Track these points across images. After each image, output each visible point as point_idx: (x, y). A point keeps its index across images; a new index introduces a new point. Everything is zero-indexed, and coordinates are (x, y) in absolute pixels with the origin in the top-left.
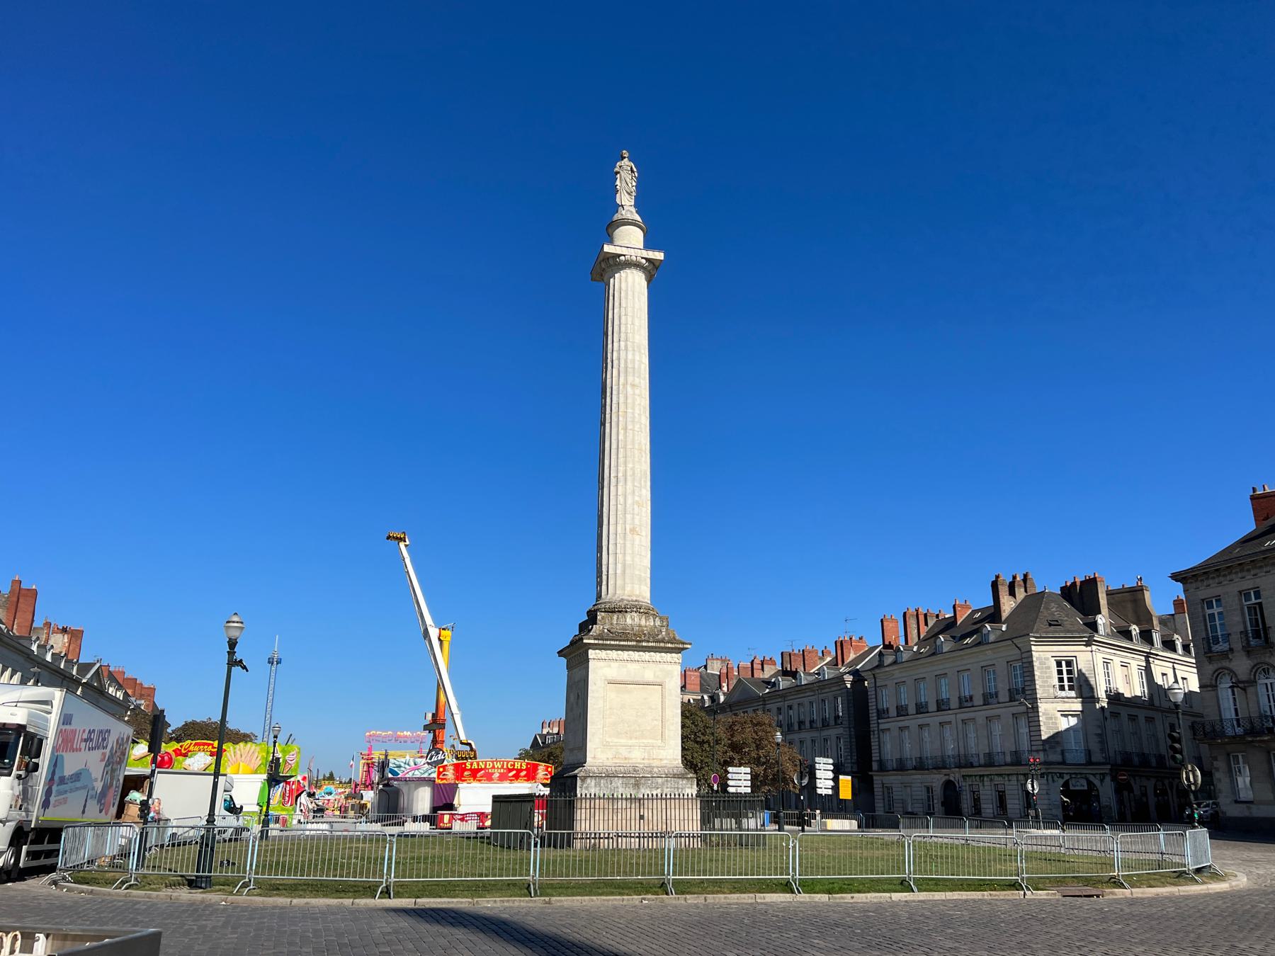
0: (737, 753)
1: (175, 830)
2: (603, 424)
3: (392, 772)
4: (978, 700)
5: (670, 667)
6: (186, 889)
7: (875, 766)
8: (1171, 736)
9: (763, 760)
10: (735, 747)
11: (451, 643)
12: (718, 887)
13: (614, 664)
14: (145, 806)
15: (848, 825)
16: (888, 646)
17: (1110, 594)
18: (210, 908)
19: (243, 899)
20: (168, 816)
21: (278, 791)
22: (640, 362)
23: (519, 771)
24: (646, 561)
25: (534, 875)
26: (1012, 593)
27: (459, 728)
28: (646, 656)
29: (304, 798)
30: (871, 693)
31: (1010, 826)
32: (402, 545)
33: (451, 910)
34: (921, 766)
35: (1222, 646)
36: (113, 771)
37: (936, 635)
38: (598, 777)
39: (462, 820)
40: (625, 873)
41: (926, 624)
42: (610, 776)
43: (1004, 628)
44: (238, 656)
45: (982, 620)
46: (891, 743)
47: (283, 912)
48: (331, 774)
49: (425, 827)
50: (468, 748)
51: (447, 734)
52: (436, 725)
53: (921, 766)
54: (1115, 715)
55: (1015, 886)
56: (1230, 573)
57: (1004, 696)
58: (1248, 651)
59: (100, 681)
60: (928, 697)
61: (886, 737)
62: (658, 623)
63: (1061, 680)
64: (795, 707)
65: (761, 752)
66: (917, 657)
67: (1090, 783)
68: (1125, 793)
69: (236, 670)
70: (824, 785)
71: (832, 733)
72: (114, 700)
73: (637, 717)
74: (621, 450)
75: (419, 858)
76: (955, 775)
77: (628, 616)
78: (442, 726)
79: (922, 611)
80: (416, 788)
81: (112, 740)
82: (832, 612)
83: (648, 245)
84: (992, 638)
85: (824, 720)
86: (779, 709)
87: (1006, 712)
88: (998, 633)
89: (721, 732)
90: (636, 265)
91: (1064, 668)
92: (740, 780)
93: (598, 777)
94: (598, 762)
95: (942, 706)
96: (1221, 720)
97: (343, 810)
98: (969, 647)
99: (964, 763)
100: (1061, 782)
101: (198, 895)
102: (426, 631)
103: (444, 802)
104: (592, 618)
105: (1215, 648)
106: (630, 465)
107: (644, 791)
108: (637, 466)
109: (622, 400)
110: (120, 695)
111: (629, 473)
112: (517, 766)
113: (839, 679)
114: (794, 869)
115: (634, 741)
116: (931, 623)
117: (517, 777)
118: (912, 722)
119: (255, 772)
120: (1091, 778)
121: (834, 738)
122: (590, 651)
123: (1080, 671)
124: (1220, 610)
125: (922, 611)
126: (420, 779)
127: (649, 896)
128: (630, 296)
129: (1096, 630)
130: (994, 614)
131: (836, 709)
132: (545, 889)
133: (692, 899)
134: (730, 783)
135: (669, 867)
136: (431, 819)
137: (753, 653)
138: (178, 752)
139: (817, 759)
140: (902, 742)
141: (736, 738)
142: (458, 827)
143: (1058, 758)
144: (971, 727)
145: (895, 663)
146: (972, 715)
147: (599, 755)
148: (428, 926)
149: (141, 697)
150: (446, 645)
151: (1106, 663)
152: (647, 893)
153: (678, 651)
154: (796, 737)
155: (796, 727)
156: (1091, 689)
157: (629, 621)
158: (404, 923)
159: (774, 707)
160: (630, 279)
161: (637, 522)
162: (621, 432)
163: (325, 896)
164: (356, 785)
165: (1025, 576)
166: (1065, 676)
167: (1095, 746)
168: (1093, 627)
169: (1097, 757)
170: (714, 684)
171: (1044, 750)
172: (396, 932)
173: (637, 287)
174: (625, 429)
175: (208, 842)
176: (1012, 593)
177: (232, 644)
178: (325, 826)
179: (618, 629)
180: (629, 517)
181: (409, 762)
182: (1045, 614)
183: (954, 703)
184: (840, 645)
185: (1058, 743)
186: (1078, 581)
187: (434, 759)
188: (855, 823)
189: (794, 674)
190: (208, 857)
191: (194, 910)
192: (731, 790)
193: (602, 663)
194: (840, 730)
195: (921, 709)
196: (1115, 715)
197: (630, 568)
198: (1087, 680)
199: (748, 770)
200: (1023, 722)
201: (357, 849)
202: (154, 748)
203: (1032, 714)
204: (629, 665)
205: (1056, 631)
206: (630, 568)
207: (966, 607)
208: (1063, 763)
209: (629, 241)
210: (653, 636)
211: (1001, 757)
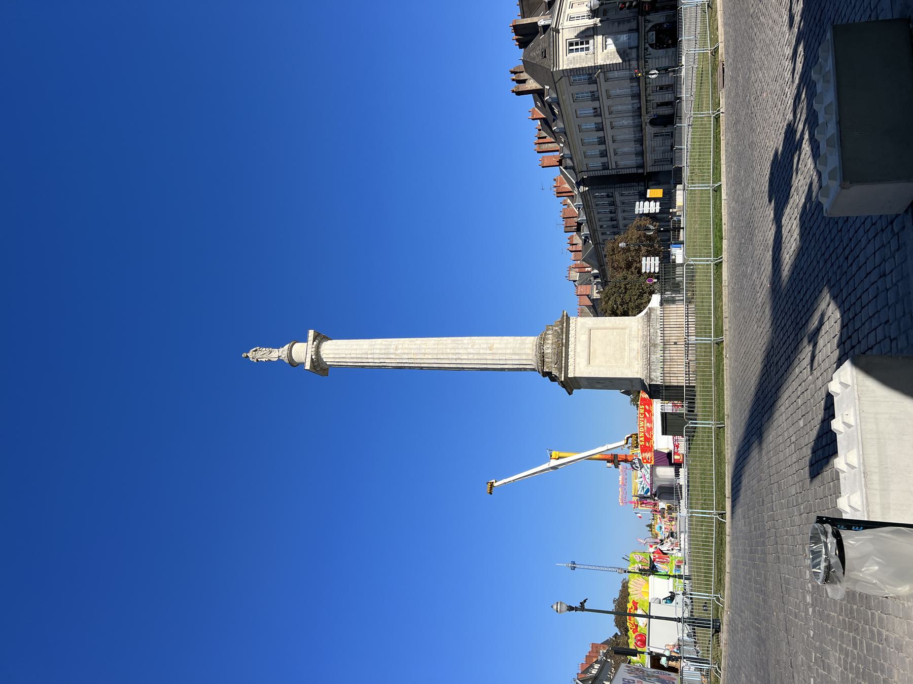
0: (632, 265)
1: (685, 635)
2: (421, 368)
3: (646, 492)
4: (596, 104)
5: (579, 325)
6: (721, 634)
7: (640, 171)
8: (621, 9)
9: (637, 247)
10: (629, 266)
11: (560, 451)
12: (718, 308)
13: (578, 360)
14: (669, 658)
16: (560, 163)
17: (523, 16)
18: (731, 622)
19: (726, 601)
20: (676, 640)
21: (659, 566)
22: (381, 344)
23: (645, 410)
24: (510, 339)
25: (712, 424)
26: (524, 81)
27: (616, 445)
28: (571, 340)
29: (664, 548)
30: (592, 174)
31: (680, 98)
32: (495, 484)
33: (732, 479)
34: (640, 141)
36: (648, 676)
37: (553, 132)
38: (650, 371)
39: (678, 447)
40: (711, 368)
41: (545, 137)
42: (649, 363)
44: (578, 605)
45: (543, 102)
46: (624, 159)
47: (734, 580)
48: (648, 526)
49: (683, 471)
50: (630, 440)
51: (621, 453)
52: (615, 460)
53: (640, 141)
54: (605, 12)
55: (717, 118)
57: (593, 87)
59: (588, 680)
60: (594, 137)
61: (622, 163)
62: (550, 332)
63: (582, 49)
64: (601, 223)
65: (632, 248)
66: (567, 144)
67: (650, 30)
68: (657, 5)
69: (586, 606)
70: (653, 208)
71: (618, 199)
72: (600, 670)
73: (609, 346)
74: (439, 356)
75: (702, 483)
76: (646, 118)
77: (546, 351)
78: (616, 456)
79: (536, 140)
80: (657, 476)
81: (629, 677)
82: (536, 204)
83: (304, 340)
84: (554, 95)
85: (610, 205)
86: (603, 234)
87: (604, 86)
88: (551, 91)
89: (619, 275)
90: (318, 348)
91: (574, 47)
92: (650, 264)
93: (650, 371)
94: (640, 370)
95: (600, 128)
97: (671, 519)
98: (560, 111)
99: (638, 112)
100: (650, 49)
101: (724, 628)
102: (553, 468)
103: (667, 459)
104: (548, 374)
106: (448, 351)
107: (659, 340)
108: (449, 346)
109: (406, 356)
110: (597, 666)
111: (453, 351)
112: (642, 411)
113: (583, 195)
114: (707, 261)
115: (627, 348)
116: (544, 134)
117: (649, 411)
118: (611, 147)
119: (648, 581)
120: (647, 29)
121: (623, 198)
122: (569, 376)
123: (576, 37)
125: (536, 140)
126: (651, 475)
127: (724, 353)
128: (339, 351)
129: (548, 26)
130: (539, 94)
131: (602, 197)
132: (720, 418)
133: (726, 327)
134: (652, 271)
135: (704, 340)
136: (678, 466)
137: (565, 251)
138: (635, 631)
139: (636, 212)
140: (625, 154)
141: (623, 265)
142: (682, 449)
143: (635, 51)
144: (614, 109)
145: (571, 159)
146: (606, 109)
147: (636, 369)
148: (741, 498)
149: (598, 652)
150: (562, 454)
151: (571, 19)
152: (722, 354)
153: (568, 319)
154: (621, 223)
155: (614, 223)
156: (588, 29)
157: (549, 351)
158: (739, 511)
159: (601, 237)
160: (327, 352)
161: (485, 346)
162: (426, 356)
163: (724, 551)
164: (656, 511)
165: (512, 72)
166: (579, 47)
167: (627, 26)
168: (546, 28)
169: (633, 25)
170: (585, 276)
171: (629, 61)
172: (744, 517)
173: (333, 347)
174: (425, 354)
175: (694, 622)
176: (524, 81)
177: (571, 608)
178: (682, 536)
179: (554, 358)
180: (482, 351)
181: (640, 481)
182: (538, 60)
183: (598, 120)
184: (560, 194)
185: (624, 52)
186: (515, 37)
187: (638, 465)
188: (679, 187)
189: (579, 225)
190: (701, 623)
191: (732, 632)
192: (657, 270)
193: (577, 369)
194: (617, 194)
195: (602, 141)
196: (605, 12)
197: (514, 350)
198: (582, 32)
199: (644, 259)
200: (610, 75)
201: (696, 521)
202: (634, 653)
203: (605, 69)
204: (578, 351)
205: (549, 53)
206: (514, 350)
207: (533, 112)
208: (638, 47)
209: (302, 352)
210: (558, 335)
211: (634, 89)
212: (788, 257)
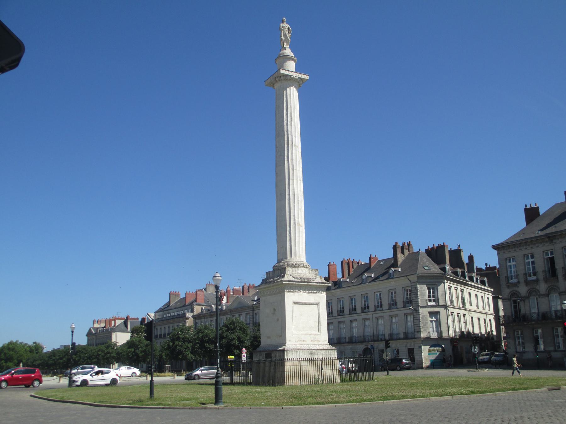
15: (123, 372)
26: (403, 253)
35: (515, 280)
43: (400, 270)
56: (520, 246)
58: (546, 280)
63: (430, 297)
96: (531, 313)
99: (376, 339)
105: (511, 281)
118: (359, 317)
124: (514, 263)
125: (351, 260)
146: (381, 315)
176: (403, 253)
212: (502, 313)
